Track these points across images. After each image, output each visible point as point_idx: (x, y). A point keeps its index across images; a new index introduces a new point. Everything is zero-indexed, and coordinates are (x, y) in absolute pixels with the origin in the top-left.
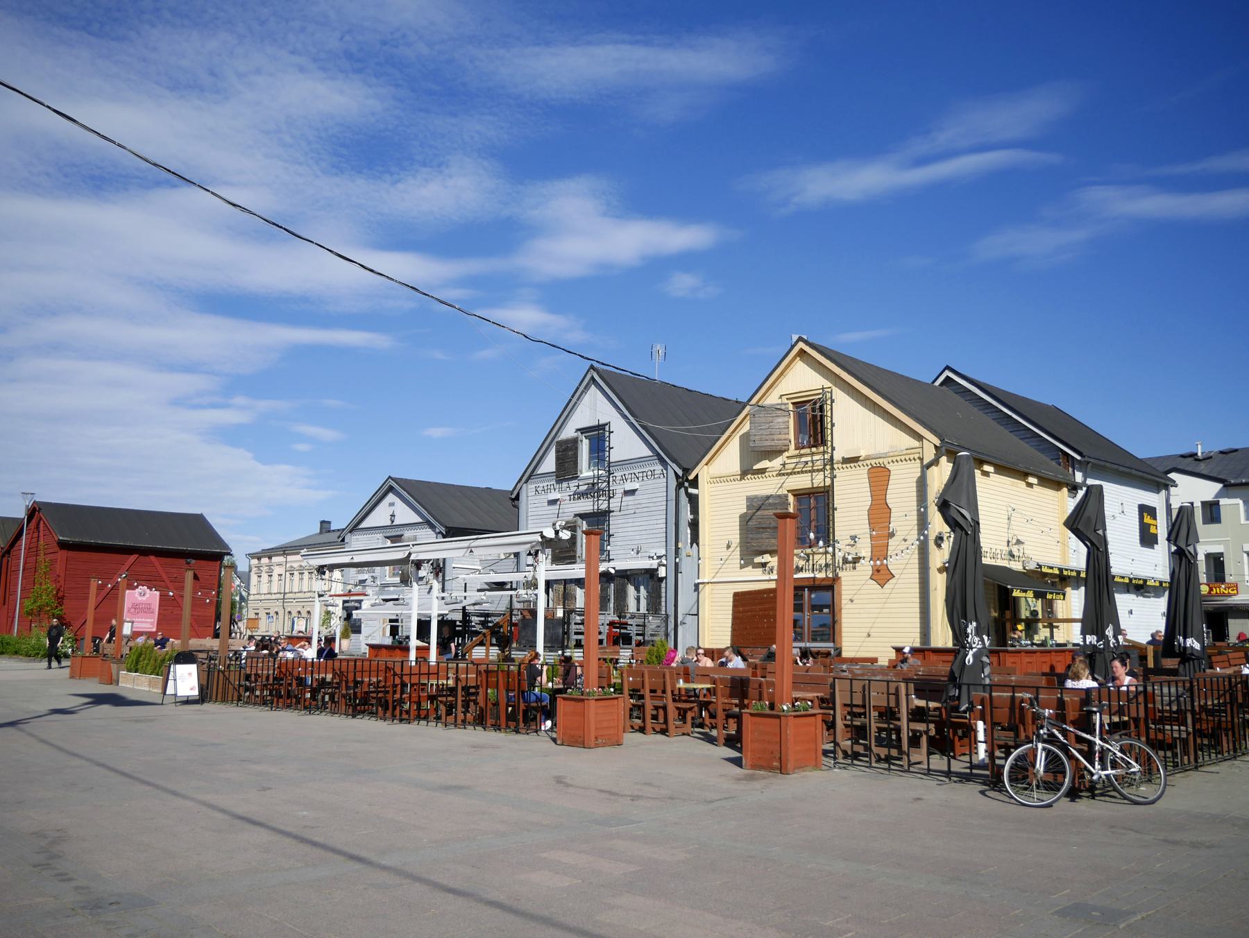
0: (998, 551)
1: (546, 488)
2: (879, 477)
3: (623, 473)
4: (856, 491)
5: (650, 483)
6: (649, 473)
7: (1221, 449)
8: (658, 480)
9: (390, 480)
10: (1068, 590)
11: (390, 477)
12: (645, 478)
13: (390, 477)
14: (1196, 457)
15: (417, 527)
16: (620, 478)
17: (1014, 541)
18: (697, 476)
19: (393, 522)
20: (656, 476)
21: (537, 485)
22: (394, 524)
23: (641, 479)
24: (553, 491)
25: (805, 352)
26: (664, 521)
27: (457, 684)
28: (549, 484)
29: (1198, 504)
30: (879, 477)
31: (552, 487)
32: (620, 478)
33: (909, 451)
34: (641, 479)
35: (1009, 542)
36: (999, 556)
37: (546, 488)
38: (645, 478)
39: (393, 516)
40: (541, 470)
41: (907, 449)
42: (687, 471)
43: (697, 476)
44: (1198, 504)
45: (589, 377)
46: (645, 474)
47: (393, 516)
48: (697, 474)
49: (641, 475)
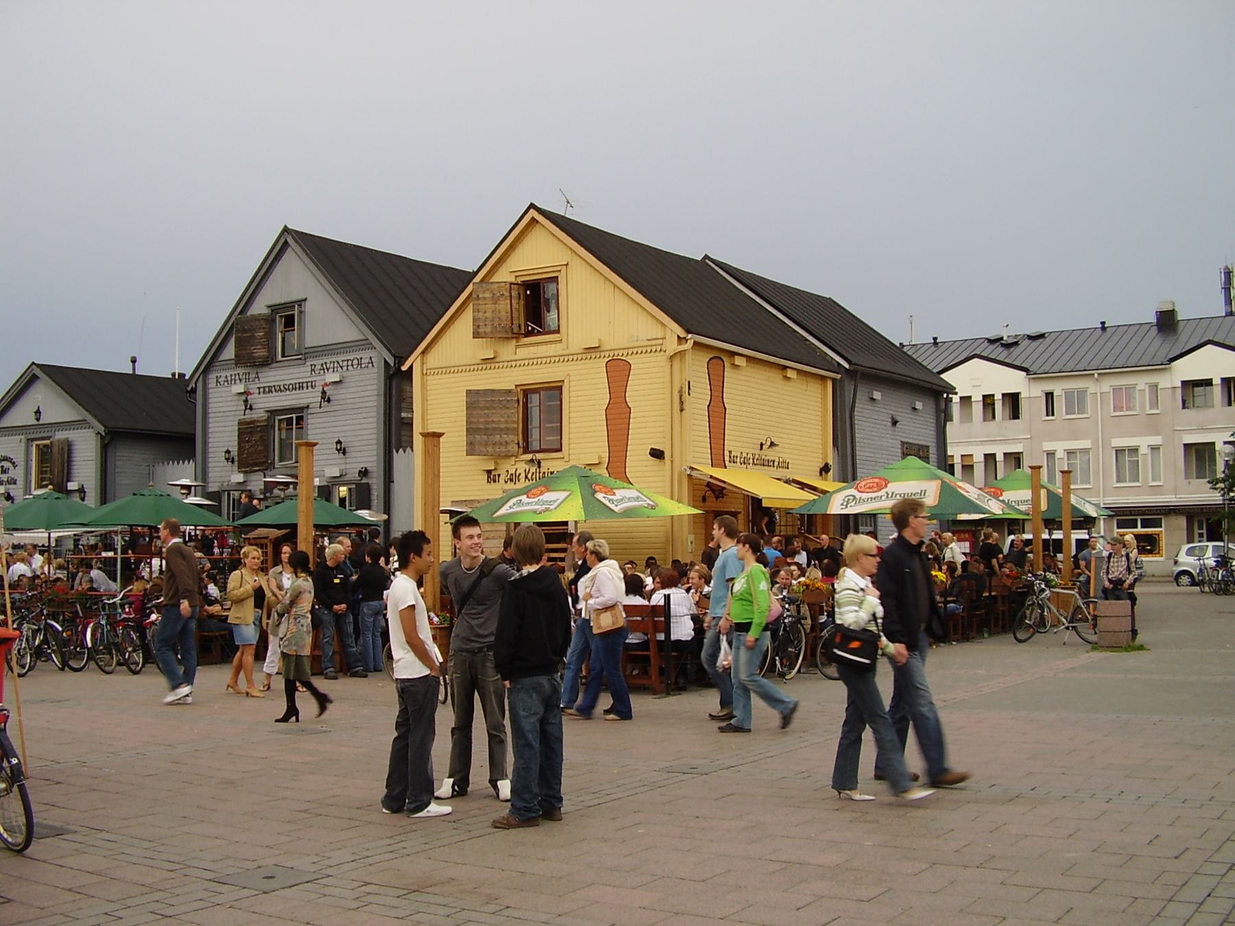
0: (750, 455)
1: (229, 378)
2: (618, 372)
3: (323, 361)
4: (351, 422)
5: (353, 375)
6: (355, 362)
7: (1028, 333)
8: (366, 371)
9: (532, 210)
10: (168, 530)
11: (532, 206)
12: (350, 368)
13: (33, 363)
14: (1003, 342)
15: (68, 427)
16: (319, 367)
17: (769, 443)
18: (411, 367)
19: (38, 420)
20: (363, 366)
21: (219, 375)
22: (41, 422)
23: (345, 368)
24: (238, 382)
25: (537, 222)
26: (571, 395)
27: (676, 679)
28: (233, 373)
29: (998, 397)
30: (618, 372)
31: (237, 377)
32: (319, 367)
33: (651, 343)
34: (345, 368)
35: (762, 445)
36: (751, 461)
37: (229, 378)
38: (350, 368)
39: (38, 412)
40: (223, 357)
41: (649, 340)
42: (400, 360)
43: (411, 367)
44: (998, 397)
45: (282, 240)
46: (350, 363)
47: (38, 412)
48: (412, 365)
49: (345, 363)
